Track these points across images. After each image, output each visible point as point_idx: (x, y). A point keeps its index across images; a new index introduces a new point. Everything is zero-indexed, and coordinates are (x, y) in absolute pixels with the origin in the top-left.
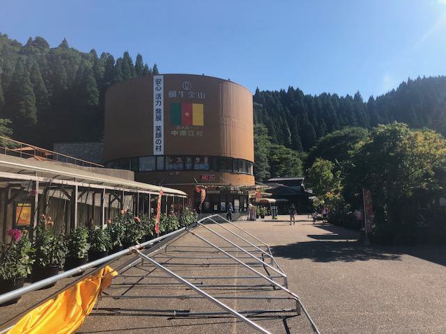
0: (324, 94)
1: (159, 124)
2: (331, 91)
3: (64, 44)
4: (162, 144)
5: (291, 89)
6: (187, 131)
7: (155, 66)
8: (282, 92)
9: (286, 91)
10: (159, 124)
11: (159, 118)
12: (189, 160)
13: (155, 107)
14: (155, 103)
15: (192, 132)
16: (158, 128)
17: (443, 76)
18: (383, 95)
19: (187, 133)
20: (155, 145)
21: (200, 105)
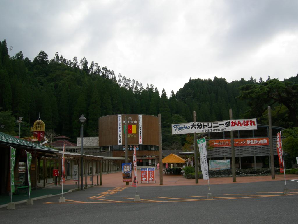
0: (199, 79)
1: (120, 133)
2: (200, 78)
3: (205, 79)
4: (121, 141)
5: (216, 78)
6: (130, 135)
7: (164, 90)
8: (210, 81)
9: (213, 81)
10: (120, 133)
11: (120, 131)
12: (131, 146)
13: (119, 127)
14: (118, 125)
15: (132, 136)
16: (120, 135)
17: (202, 80)
18: (200, 79)
19: (130, 136)
20: (119, 141)
21: (135, 125)
